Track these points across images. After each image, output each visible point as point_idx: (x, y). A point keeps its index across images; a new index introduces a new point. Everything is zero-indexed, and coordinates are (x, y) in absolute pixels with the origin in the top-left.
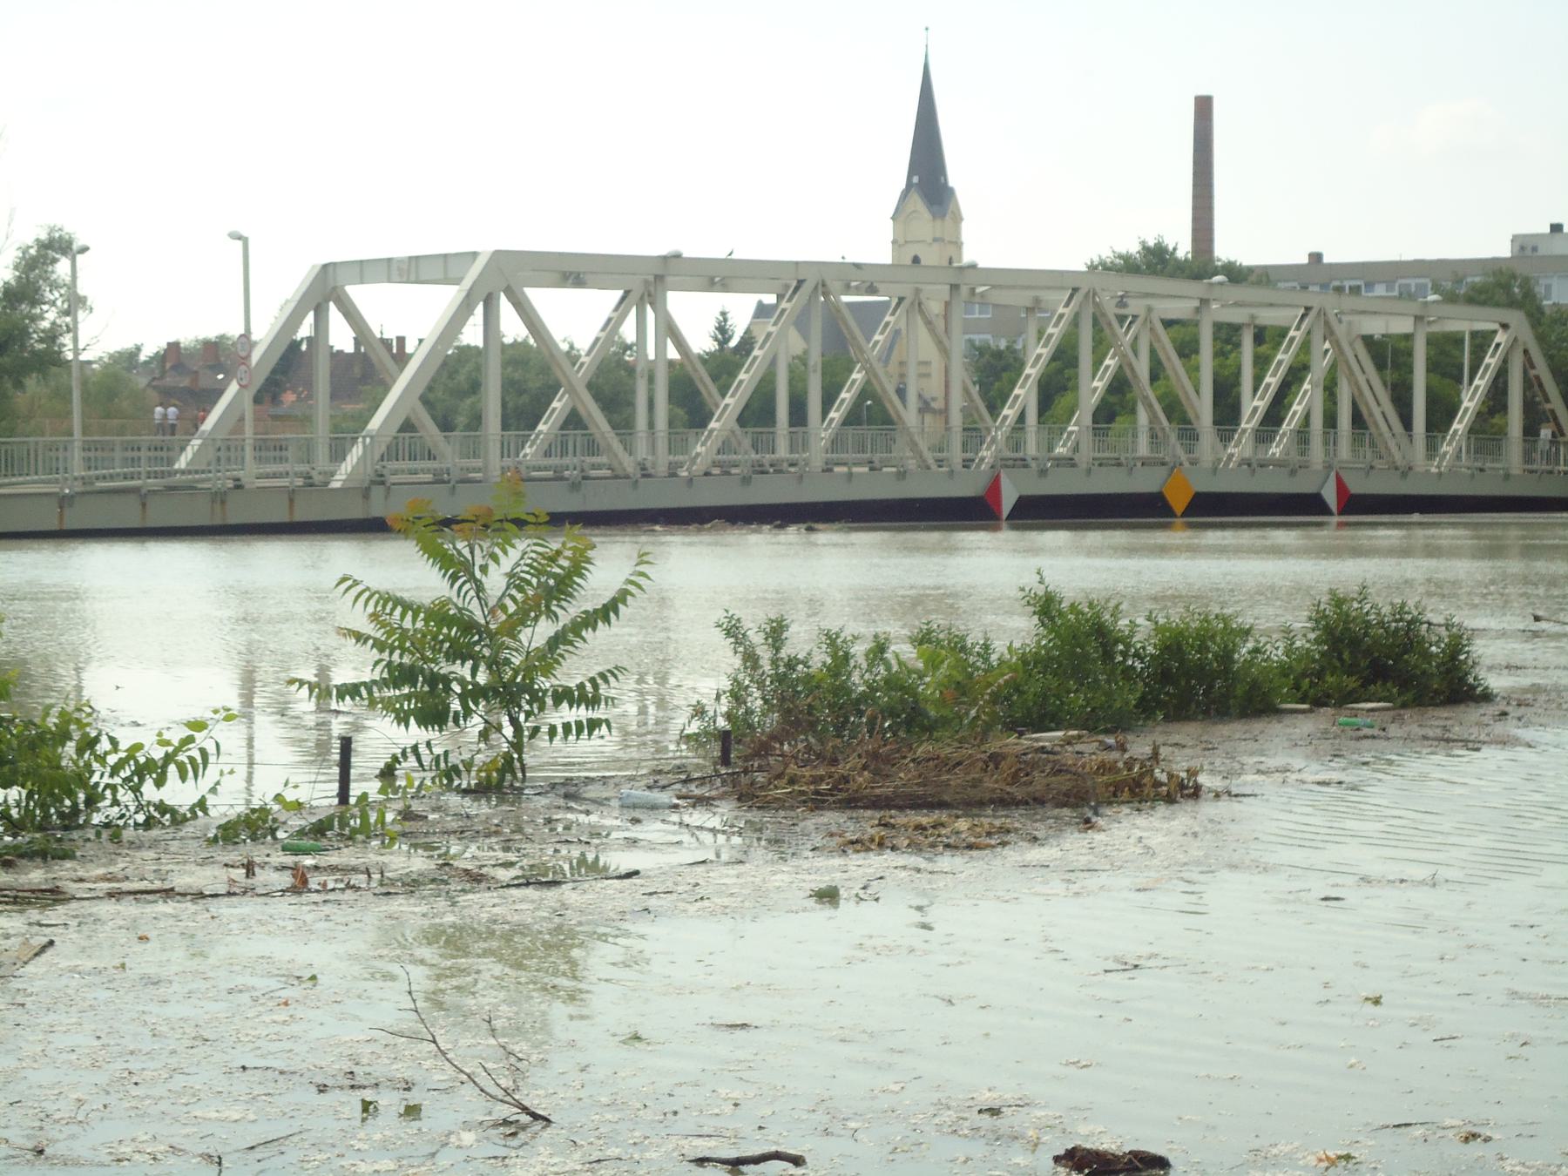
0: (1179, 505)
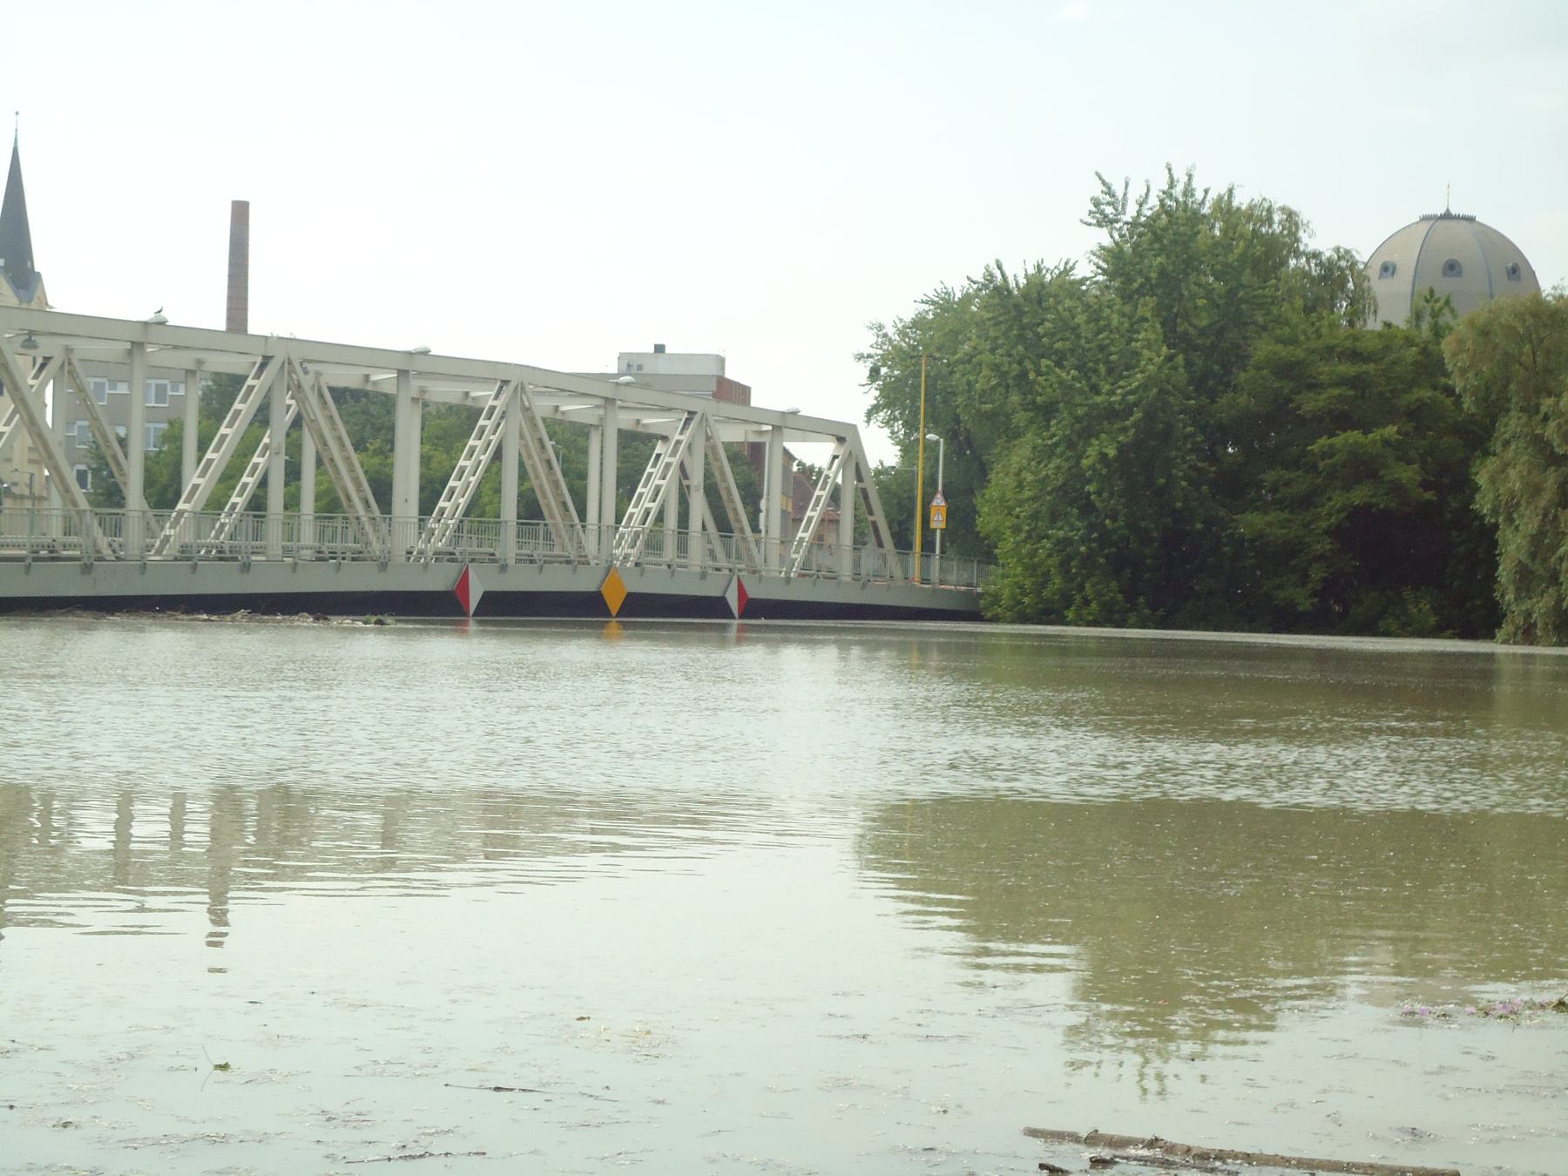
0: (614, 604)
